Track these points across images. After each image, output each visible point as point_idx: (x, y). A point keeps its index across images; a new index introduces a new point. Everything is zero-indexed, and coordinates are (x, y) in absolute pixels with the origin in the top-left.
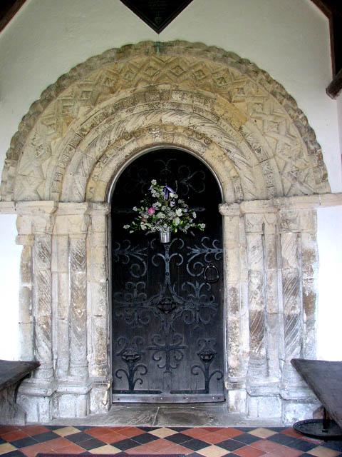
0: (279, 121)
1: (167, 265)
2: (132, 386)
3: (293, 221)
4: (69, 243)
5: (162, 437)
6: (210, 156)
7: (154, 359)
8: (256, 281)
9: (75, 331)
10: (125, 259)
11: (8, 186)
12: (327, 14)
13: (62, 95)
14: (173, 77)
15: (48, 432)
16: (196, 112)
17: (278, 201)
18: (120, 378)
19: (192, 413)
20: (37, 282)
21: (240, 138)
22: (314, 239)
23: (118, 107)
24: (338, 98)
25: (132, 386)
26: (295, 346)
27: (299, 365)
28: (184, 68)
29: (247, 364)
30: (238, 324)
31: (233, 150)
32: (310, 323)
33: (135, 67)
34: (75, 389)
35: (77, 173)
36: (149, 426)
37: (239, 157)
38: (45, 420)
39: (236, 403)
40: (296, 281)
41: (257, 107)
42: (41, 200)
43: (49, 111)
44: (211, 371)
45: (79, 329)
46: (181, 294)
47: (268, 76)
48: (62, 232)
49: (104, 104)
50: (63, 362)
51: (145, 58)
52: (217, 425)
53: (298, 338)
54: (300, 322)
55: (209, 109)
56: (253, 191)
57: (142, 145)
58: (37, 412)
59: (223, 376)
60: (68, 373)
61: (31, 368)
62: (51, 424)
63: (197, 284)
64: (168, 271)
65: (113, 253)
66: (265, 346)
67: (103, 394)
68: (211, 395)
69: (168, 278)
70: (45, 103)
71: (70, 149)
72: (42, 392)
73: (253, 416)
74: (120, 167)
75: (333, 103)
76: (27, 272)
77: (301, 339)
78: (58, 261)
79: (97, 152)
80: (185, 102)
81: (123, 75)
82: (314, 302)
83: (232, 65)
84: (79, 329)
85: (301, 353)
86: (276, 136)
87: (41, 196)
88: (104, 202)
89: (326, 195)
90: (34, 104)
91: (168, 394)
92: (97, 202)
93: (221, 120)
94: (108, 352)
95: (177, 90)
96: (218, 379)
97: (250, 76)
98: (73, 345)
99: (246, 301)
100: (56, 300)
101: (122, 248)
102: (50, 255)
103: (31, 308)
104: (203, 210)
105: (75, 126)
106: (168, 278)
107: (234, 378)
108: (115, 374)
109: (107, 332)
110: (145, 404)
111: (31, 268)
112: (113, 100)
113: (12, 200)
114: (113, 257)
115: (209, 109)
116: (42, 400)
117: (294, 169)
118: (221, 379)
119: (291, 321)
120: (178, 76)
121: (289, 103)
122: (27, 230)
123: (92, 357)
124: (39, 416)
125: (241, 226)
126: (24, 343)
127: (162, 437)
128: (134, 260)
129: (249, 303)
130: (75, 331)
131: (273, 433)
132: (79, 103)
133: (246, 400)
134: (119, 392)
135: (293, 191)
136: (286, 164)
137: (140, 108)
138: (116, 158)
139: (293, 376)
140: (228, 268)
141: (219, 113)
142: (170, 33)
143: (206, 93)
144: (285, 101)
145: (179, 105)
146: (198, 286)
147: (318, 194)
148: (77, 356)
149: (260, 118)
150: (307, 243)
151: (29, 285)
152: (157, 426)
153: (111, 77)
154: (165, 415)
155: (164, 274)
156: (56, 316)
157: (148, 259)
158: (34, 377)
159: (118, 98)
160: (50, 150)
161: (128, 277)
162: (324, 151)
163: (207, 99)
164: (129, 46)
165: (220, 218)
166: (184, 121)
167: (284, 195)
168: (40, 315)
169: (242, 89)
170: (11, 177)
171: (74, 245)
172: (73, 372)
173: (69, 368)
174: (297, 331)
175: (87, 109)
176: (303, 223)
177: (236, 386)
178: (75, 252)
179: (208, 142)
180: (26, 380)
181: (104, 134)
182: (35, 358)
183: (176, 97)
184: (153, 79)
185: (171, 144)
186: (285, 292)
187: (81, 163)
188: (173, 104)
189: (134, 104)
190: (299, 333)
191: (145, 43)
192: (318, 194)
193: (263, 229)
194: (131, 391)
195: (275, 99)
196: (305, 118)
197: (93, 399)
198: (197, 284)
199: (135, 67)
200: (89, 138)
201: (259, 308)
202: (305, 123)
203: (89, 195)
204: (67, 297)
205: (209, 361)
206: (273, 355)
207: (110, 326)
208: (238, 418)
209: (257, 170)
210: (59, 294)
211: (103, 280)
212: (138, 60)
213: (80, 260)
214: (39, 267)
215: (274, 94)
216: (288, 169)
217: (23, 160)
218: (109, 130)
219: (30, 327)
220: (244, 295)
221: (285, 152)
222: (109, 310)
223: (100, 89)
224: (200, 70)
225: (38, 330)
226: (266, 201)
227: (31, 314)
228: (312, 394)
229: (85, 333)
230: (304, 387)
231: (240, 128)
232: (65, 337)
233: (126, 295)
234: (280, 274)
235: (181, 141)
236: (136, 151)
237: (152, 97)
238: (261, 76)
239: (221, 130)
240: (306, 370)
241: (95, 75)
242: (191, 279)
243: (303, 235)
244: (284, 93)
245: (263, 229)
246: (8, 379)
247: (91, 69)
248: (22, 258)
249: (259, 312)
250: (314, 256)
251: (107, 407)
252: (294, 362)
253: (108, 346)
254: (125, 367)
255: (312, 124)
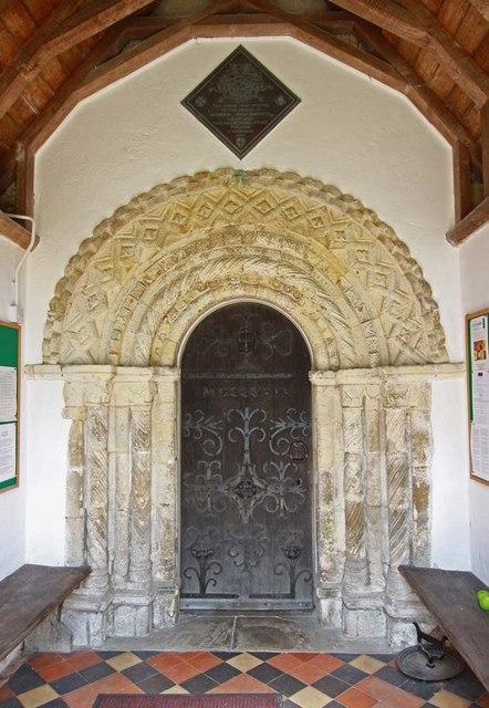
2: (203, 588)
3: (402, 396)
4: (130, 416)
5: (244, 669)
6: (295, 314)
7: (230, 555)
8: (354, 466)
9: (137, 526)
10: (197, 433)
12: (450, 141)
13: (121, 232)
14: (258, 215)
15: (97, 664)
17: (385, 371)
18: (190, 578)
19: (277, 626)
20: (89, 465)
21: (339, 292)
22: (427, 418)
24: (461, 246)
25: (203, 588)
26: (403, 549)
27: (409, 572)
28: (272, 205)
29: (342, 566)
30: (331, 516)
31: (326, 305)
32: (422, 521)
34: (135, 600)
35: (139, 330)
36: (226, 650)
37: (336, 315)
38: (97, 643)
40: (404, 469)
41: (359, 255)
42: (95, 363)
43: (102, 252)
44: (298, 570)
45: (142, 523)
46: (261, 476)
47: (375, 217)
48: (120, 403)
49: (174, 246)
50: (122, 565)
51: (224, 190)
52: (310, 649)
53: (406, 539)
54: (409, 519)
55: (301, 257)
56: (352, 356)
57: (218, 297)
58: (86, 631)
59: (311, 577)
60: (128, 578)
61: (85, 572)
62: (103, 649)
63: (282, 464)
64: (247, 447)
65: (182, 425)
66: (364, 546)
67: (170, 603)
68: (297, 601)
69: (247, 456)
70: (98, 242)
71: (132, 301)
72: (93, 607)
74: (192, 324)
76: (78, 452)
77: (411, 541)
78: (116, 437)
80: (272, 246)
81: (196, 210)
83: (331, 202)
84: (142, 523)
85: (411, 558)
86: (383, 292)
87: (95, 357)
88: (172, 367)
89: (444, 366)
90: (85, 243)
91: (245, 599)
92: (166, 366)
93: (315, 270)
94: (176, 548)
95: (263, 232)
96: (306, 581)
97: (353, 216)
98: (133, 542)
99: (341, 488)
100: (113, 487)
101: (196, 418)
102: (106, 432)
103: (81, 499)
104: (289, 375)
106: (247, 456)
107: (327, 584)
108: (183, 573)
111: (82, 449)
112: (184, 241)
113: (58, 363)
114: (183, 432)
115: (301, 257)
116: (93, 616)
117: (404, 332)
118: (310, 580)
119: (398, 518)
120: (265, 215)
121: (401, 251)
123: (155, 556)
124: (89, 637)
126: (71, 543)
127: (244, 669)
128: (207, 434)
129: (346, 492)
130: (137, 526)
131: (381, 665)
132: (141, 245)
133: (342, 612)
134: (188, 596)
135: (402, 360)
136: (394, 326)
138: (187, 313)
139: (402, 589)
140: (172, 394)
141: (313, 262)
142: (254, 159)
143: (299, 236)
144: (396, 249)
145: (265, 250)
146: (282, 467)
147: (432, 363)
148: (139, 556)
149: (364, 269)
150: (419, 423)
151: (80, 470)
152: (236, 650)
153: (182, 212)
154: (245, 630)
155: (243, 451)
156: (113, 506)
158: (84, 587)
159: (191, 239)
161: (200, 456)
162: (442, 310)
163: (298, 243)
164: (205, 173)
166: (267, 271)
167: (390, 365)
169: (343, 232)
170: (56, 335)
171: (136, 417)
172: (134, 577)
173: (129, 571)
174: (405, 530)
177: (329, 594)
178: (138, 427)
179: (297, 298)
180: (75, 591)
181: (174, 283)
182: (86, 562)
183: (261, 242)
184: (235, 217)
185: (254, 297)
186: (390, 483)
187: (144, 319)
188: (258, 249)
189: (209, 247)
190: (408, 533)
191: (225, 170)
192: (432, 363)
193: (364, 404)
194: (203, 595)
195: (383, 246)
196: (420, 270)
197: (157, 609)
198: (282, 464)
200: (155, 288)
201: (358, 499)
202: (419, 276)
203: (156, 357)
204: (126, 483)
206: (375, 556)
207: (178, 518)
208: (333, 637)
209: (357, 332)
210: (117, 479)
211: (171, 461)
212: (215, 191)
213: (144, 437)
214: (93, 447)
215: (381, 238)
217: (72, 313)
218: (180, 279)
219: (80, 523)
222: (178, 497)
223: (169, 228)
224: (292, 208)
225: (91, 526)
226: (368, 370)
227: (81, 506)
228: (426, 612)
229: (149, 527)
230: (415, 602)
231: (339, 281)
232: (124, 533)
233: (197, 477)
235: (265, 297)
236: (211, 304)
237: (231, 242)
239: (314, 282)
240: (416, 576)
242: (274, 458)
243: (414, 413)
244: (394, 238)
245: (364, 404)
246: (49, 602)
248: (70, 436)
249: (359, 504)
250: (427, 439)
251: (173, 619)
252: (401, 568)
253: (176, 382)
254: (196, 565)
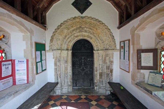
0: (107, 34)
1: (83, 62)
2: (76, 85)
3: (109, 55)
4: (64, 58)
6: (91, 41)
8: (101, 66)
11: (51, 47)
13: (62, 27)
16: (89, 32)
20: (58, 67)
22: (113, 58)
23: (73, 31)
24: (119, 29)
25: (76, 85)
32: (112, 75)
33: (77, 22)
34: (66, 87)
38: (60, 94)
39: (96, 89)
40: (109, 67)
42: (58, 50)
46: (85, 68)
48: (62, 56)
49: (70, 30)
50: (63, 82)
51: (79, 20)
52: (93, 95)
55: (92, 31)
56: (101, 48)
60: (64, 84)
61: (57, 83)
70: (58, 29)
73: (100, 92)
75: (118, 30)
76: (56, 64)
79: (69, 40)
82: (112, 71)
83: (97, 22)
88: (71, 50)
90: (56, 29)
91: (83, 87)
95: (86, 27)
100: (61, 70)
102: (60, 61)
105: (65, 34)
107: (96, 85)
109: (72, 75)
110: (79, 89)
112: (72, 29)
115: (92, 31)
116: (59, 90)
122: (55, 56)
123: (69, 80)
125: (98, 55)
134: (74, 86)
135: (109, 49)
137: (78, 31)
139: (108, 85)
141: (94, 32)
143: (92, 28)
144: (108, 30)
145: (86, 30)
146: (89, 66)
150: (111, 59)
156: (62, 73)
157: (79, 61)
160: (59, 39)
163: (92, 29)
165: (93, 53)
167: (107, 50)
168: (59, 73)
170: (51, 45)
172: (65, 84)
175: (67, 31)
176: (111, 56)
179: (91, 38)
183: (85, 29)
186: (106, 69)
187: (66, 42)
191: (79, 16)
194: (76, 86)
196: (112, 34)
199: (77, 22)
200: (67, 37)
205: (91, 80)
208: (97, 93)
211: (71, 65)
212: (77, 20)
214: (58, 64)
216: (108, 44)
217: (54, 41)
219: (56, 76)
220: (98, 69)
221: (108, 41)
225: (58, 76)
229: (67, 76)
230: (110, 88)
231: (99, 36)
234: (105, 65)
235: (86, 38)
237: (80, 29)
238: (104, 25)
241: (68, 23)
247: (68, 22)
255: (113, 35)
